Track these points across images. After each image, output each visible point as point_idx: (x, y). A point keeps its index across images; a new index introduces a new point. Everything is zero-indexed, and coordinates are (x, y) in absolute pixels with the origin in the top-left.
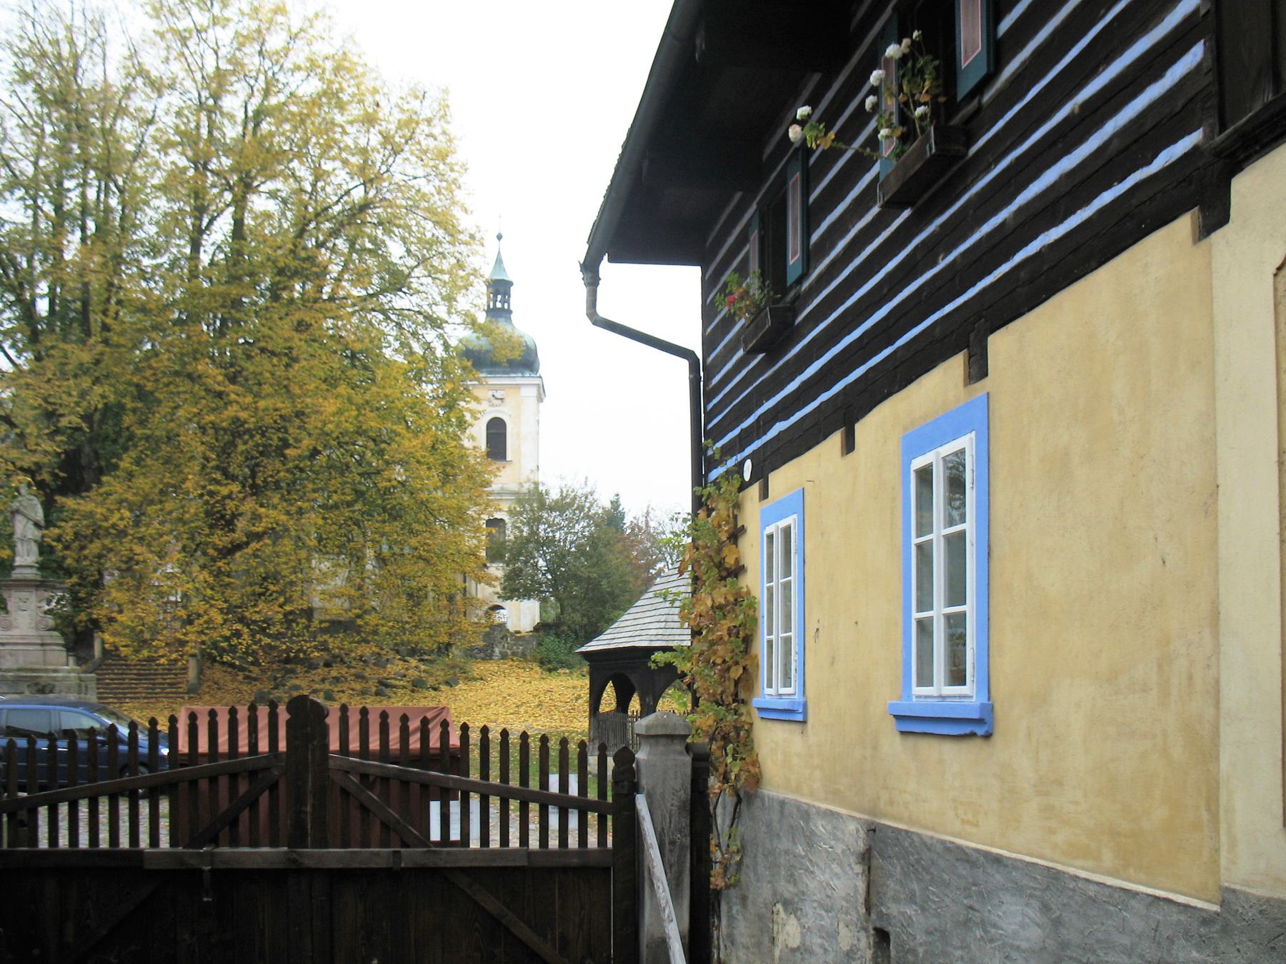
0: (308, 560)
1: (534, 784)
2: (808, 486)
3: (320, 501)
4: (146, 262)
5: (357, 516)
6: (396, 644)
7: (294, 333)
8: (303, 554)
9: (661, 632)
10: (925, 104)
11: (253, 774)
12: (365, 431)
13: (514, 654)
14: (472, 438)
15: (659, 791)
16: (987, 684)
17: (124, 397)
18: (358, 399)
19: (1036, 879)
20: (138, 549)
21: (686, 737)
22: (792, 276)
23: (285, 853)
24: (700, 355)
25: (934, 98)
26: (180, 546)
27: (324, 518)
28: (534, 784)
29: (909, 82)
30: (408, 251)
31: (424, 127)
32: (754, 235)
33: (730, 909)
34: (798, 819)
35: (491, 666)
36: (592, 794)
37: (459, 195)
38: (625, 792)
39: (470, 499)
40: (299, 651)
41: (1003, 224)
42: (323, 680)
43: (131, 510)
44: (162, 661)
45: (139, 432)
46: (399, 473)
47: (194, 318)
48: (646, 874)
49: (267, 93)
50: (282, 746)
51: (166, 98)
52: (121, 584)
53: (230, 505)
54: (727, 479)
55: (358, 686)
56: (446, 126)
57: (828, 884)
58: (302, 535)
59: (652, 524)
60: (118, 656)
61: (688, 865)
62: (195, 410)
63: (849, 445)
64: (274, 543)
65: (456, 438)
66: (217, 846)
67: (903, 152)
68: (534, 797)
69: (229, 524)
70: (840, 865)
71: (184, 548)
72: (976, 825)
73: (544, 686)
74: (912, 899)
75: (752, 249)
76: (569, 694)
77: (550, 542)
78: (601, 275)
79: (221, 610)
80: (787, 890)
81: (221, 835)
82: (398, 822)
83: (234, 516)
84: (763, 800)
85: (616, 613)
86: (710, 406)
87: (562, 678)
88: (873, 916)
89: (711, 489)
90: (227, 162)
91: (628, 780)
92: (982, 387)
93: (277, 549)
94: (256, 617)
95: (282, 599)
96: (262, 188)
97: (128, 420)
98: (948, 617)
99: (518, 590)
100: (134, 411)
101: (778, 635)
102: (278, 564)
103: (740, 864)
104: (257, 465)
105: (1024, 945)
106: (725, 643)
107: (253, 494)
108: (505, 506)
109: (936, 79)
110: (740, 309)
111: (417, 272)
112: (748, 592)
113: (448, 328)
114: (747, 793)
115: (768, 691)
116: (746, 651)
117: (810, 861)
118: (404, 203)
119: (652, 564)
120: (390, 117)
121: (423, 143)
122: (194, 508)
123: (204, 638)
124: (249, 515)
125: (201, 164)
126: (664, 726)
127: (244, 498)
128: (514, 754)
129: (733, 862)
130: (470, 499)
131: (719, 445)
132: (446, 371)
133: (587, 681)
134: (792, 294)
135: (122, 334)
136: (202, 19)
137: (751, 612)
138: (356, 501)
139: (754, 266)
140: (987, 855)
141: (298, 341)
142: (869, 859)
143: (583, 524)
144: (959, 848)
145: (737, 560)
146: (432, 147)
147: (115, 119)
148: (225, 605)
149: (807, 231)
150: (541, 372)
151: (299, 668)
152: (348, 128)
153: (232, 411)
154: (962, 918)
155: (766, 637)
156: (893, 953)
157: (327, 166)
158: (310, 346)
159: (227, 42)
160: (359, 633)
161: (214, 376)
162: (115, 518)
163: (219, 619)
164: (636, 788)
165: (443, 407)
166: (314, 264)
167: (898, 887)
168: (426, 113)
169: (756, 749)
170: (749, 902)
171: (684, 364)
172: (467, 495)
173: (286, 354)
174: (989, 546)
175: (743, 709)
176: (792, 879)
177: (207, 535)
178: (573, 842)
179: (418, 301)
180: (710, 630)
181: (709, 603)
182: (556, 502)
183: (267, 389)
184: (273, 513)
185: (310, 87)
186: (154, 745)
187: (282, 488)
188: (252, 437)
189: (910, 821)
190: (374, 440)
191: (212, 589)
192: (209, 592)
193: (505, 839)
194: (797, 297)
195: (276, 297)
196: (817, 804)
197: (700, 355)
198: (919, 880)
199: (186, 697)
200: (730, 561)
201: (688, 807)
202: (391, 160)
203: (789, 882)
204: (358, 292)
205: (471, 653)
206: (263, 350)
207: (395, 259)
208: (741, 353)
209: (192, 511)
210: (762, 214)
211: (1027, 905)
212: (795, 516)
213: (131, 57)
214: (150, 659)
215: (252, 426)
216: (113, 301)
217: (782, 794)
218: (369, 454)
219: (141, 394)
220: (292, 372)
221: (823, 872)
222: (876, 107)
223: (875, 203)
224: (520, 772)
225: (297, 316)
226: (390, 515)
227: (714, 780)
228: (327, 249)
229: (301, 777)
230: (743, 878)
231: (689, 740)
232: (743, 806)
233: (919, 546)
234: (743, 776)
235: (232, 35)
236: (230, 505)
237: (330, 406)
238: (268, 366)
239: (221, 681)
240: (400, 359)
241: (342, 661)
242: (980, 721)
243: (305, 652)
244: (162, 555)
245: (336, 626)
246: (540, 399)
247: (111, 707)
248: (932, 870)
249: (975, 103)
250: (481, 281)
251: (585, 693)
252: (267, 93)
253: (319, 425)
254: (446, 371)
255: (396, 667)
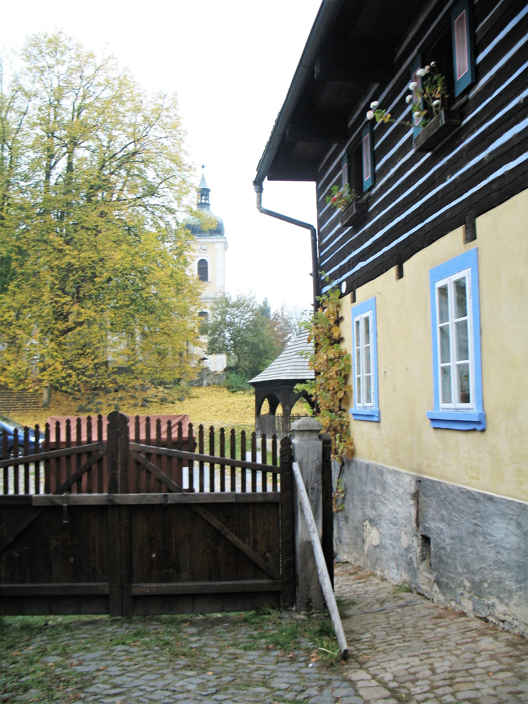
0: (106, 335)
1: (238, 458)
2: (378, 296)
3: (112, 305)
4: (22, 183)
5: (132, 312)
6: (152, 379)
7: (99, 218)
8: (104, 333)
9: (293, 371)
10: (438, 99)
11: (89, 454)
12: (136, 268)
13: (214, 383)
14: (191, 270)
15: (305, 460)
16: (482, 402)
17: (11, 253)
18: (133, 251)
19: (513, 509)
20: (18, 332)
21: (319, 431)
22: (366, 187)
23: (107, 496)
24: (316, 227)
25: (443, 95)
26: (40, 329)
27: (115, 314)
28: (238, 458)
29: (429, 87)
30: (158, 175)
31: (165, 113)
32: (345, 165)
33: (338, 524)
34: (376, 475)
35: (202, 390)
36: (269, 463)
37: (183, 146)
38: (287, 461)
39: (191, 302)
40: (102, 384)
41: (482, 160)
42: (114, 399)
43: (14, 311)
44: (31, 390)
45: (19, 271)
46: (153, 289)
47: (47, 212)
48: (299, 506)
49: (84, 97)
50: (105, 438)
51: (33, 101)
52: (9, 350)
53: (66, 308)
54: (333, 292)
55: (132, 402)
56: (176, 112)
57: (395, 511)
58: (103, 322)
59: (285, 314)
60: (7, 388)
61: (321, 501)
62: (48, 259)
63: (400, 275)
64: (89, 326)
65: (183, 270)
66: (70, 493)
67: (426, 124)
68: (238, 464)
69: (65, 318)
70: (401, 500)
71: (42, 331)
72: (478, 479)
73: (230, 400)
74: (442, 519)
75: (344, 172)
76: (244, 405)
77: (232, 324)
78: (264, 187)
79: (61, 362)
80: (371, 513)
81: (73, 486)
82: (166, 479)
83: (68, 313)
84: (356, 463)
85: (267, 361)
86: (322, 253)
87: (239, 396)
88: (421, 529)
89: (324, 297)
90: (64, 132)
91: (288, 454)
92: (473, 245)
93: (90, 330)
94: (80, 366)
95: (93, 357)
96: (82, 145)
97: (14, 264)
98: (459, 366)
99: (215, 350)
100: (16, 260)
101: (363, 375)
102: (91, 338)
103: (344, 498)
104: (80, 287)
105: (508, 546)
106: (334, 379)
107: (78, 302)
108: (208, 305)
109: (443, 86)
110: (339, 204)
111: (162, 186)
112: (346, 352)
113: (178, 214)
114: (347, 462)
115: (358, 405)
116: (345, 383)
117: (384, 497)
118: (155, 151)
119: (285, 336)
120: (148, 108)
121: (165, 120)
122: (48, 310)
123: (52, 378)
124: (76, 313)
125: (51, 134)
126: (307, 425)
127: (73, 304)
128: (217, 438)
129: (340, 497)
130: (191, 302)
131: (328, 274)
132: (177, 235)
133: (253, 398)
134: (367, 196)
135: (11, 221)
136: (51, 61)
137: (348, 362)
138: (131, 304)
139: (345, 181)
140: (485, 496)
141: (101, 222)
142: (418, 497)
143: (250, 314)
144: (468, 491)
145: (339, 335)
146: (169, 122)
147: (7, 112)
148: (63, 360)
149: (374, 164)
150: (225, 235)
151: (101, 393)
152: (127, 114)
153: (67, 259)
154: (471, 530)
155: (357, 376)
156: (432, 549)
157: (115, 133)
158: (107, 224)
159: (64, 72)
160: (133, 373)
161: (58, 241)
162: (6, 316)
163: (60, 367)
164: (292, 459)
165: (176, 254)
166: (109, 183)
167: (434, 513)
168: (166, 106)
169: (352, 436)
170: (350, 520)
171: (308, 232)
172: (188, 300)
173: (94, 229)
174: (481, 328)
175: (344, 415)
176: (374, 507)
177: (54, 324)
178: (259, 489)
179: (162, 200)
180: (326, 372)
181: (325, 358)
182: (235, 303)
183: (85, 247)
184: (88, 311)
185: (107, 94)
186: (26, 435)
187: (92, 298)
188: (77, 272)
189: (441, 477)
190: (140, 272)
191: (56, 352)
192: (55, 354)
193: (223, 488)
194: (369, 198)
195: (89, 200)
196: (387, 466)
197: (316, 227)
198: (447, 509)
199: (42, 409)
200: (336, 335)
201: (321, 469)
202: (148, 129)
203: (372, 509)
204: (131, 196)
205: (191, 384)
206: (82, 227)
207: (150, 179)
208: (339, 226)
209: (46, 311)
210: (349, 155)
211: (509, 523)
212: (371, 311)
213: (15, 81)
214: (24, 390)
215: (77, 266)
216: (5, 204)
217: (367, 461)
218: (137, 280)
219: (21, 252)
220: (98, 238)
221: (392, 504)
222: (411, 100)
223: (411, 149)
224: (227, 449)
225: (101, 209)
226: (149, 311)
227: (332, 453)
228: (115, 175)
229: (113, 455)
230: (346, 506)
231: (321, 432)
232: (345, 467)
233: (441, 329)
234: (345, 451)
235: (66, 69)
236: (66, 308)
237: (118, 255)
238: (86, 236)
239: (60, 401)
240: (154, 230)
241: (124, 389)
242: (479, 423)
243: (104, 384)
244: (30, 335)
245: (121, 370)
246: (225, 249)
247: (3, 415)
248: (454, 503)
249: (464, 99)
250: (194, 189)
251: (253, 404)
252: (84, 97)
253: (112, 265)
254: (177, 235)
255: (152, 392)
